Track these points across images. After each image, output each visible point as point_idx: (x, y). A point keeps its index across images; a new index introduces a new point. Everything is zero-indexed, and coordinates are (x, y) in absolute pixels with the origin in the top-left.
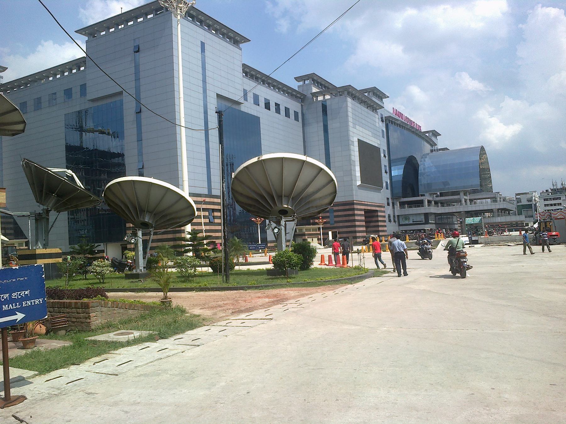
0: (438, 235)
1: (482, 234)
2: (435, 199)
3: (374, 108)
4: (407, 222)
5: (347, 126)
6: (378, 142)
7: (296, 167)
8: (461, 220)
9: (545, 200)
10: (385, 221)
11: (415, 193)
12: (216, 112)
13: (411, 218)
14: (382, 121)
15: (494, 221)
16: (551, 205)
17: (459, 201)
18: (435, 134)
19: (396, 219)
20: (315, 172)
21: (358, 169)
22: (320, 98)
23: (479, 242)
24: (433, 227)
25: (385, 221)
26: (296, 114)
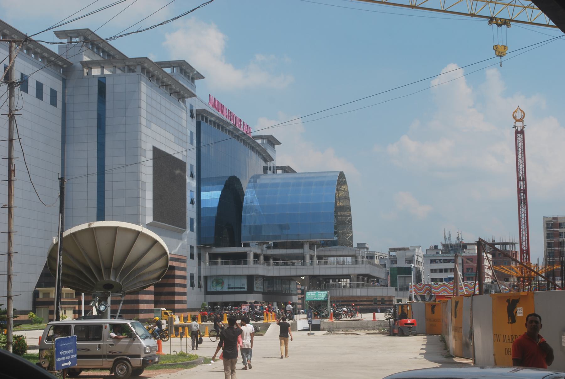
0: (267, 314)
1: (326, 317)
2: (265, 253)
3: (181, 95)
4: (219, 289)
5: (138, 124)
6: (184, 152)
7: (131, 237)
8: (303, 288)
9: (432, 261)
10: (184, 286)
11: (235, 241)
12: (59, 179)
13: (226, 282)
14: (192, 116)
15: (351, 294)
16: (441, 271)
17: (302, 257)
18: (272, 141)
19: (202, 283)
20: (149, 243)
21: (149, 196)
22: (96, 72)
23: (322, 327)
24: (258, 297)
25: (184, 286)
26: (53, 93)
